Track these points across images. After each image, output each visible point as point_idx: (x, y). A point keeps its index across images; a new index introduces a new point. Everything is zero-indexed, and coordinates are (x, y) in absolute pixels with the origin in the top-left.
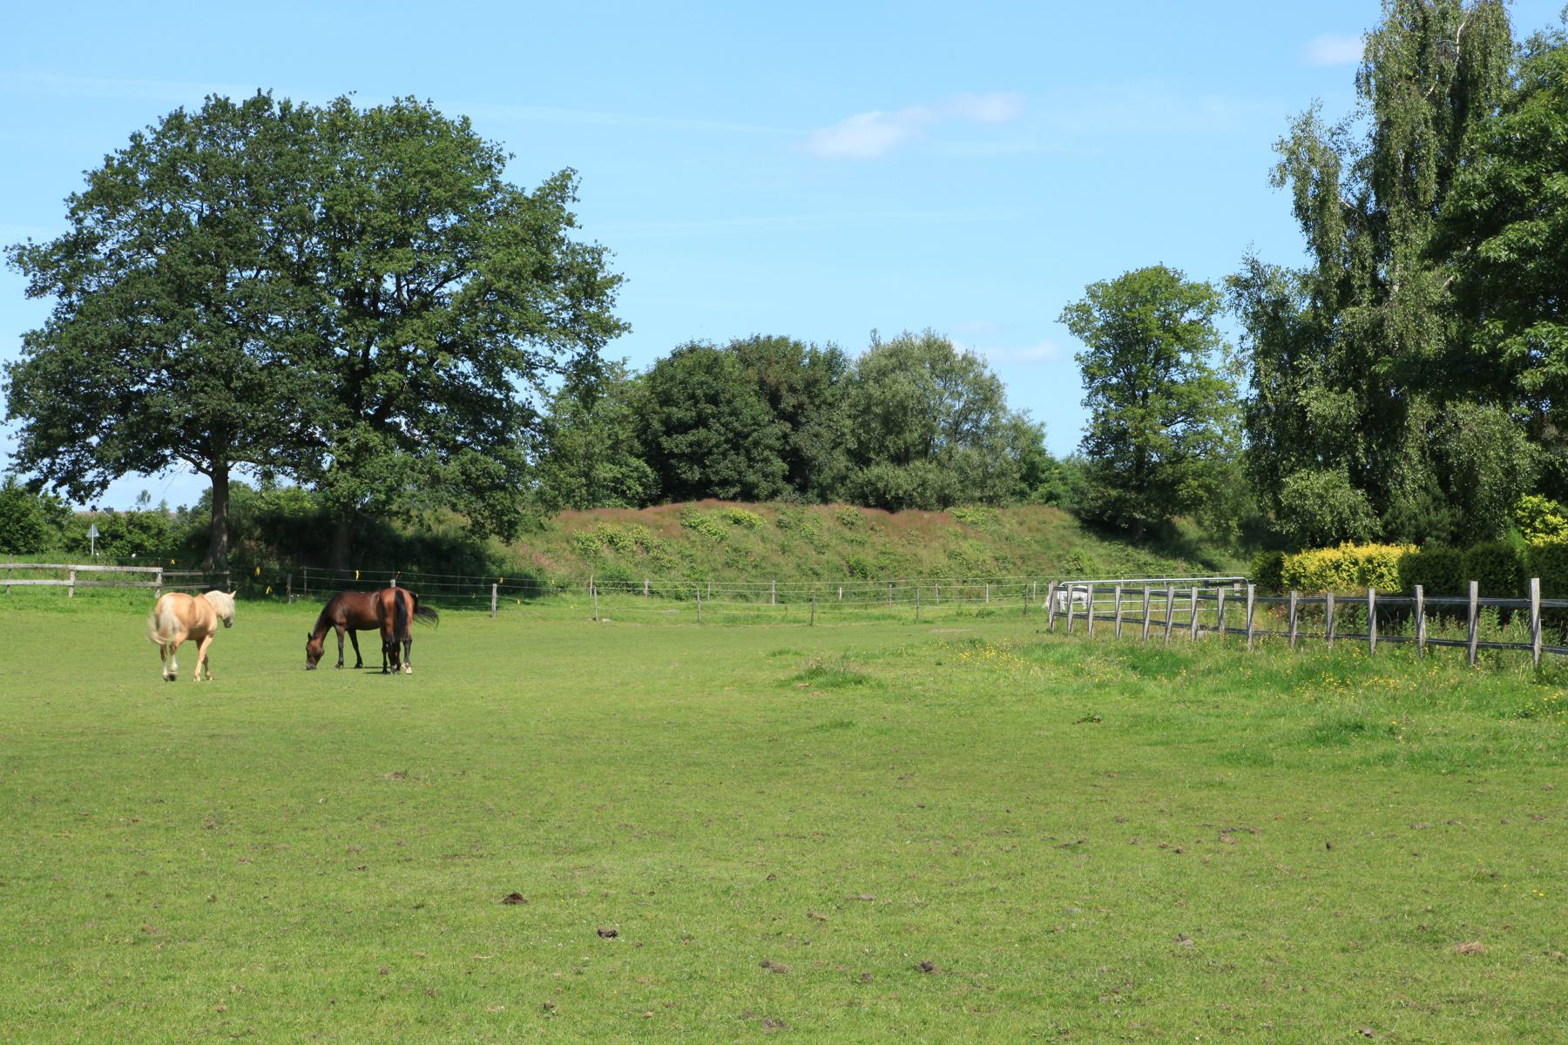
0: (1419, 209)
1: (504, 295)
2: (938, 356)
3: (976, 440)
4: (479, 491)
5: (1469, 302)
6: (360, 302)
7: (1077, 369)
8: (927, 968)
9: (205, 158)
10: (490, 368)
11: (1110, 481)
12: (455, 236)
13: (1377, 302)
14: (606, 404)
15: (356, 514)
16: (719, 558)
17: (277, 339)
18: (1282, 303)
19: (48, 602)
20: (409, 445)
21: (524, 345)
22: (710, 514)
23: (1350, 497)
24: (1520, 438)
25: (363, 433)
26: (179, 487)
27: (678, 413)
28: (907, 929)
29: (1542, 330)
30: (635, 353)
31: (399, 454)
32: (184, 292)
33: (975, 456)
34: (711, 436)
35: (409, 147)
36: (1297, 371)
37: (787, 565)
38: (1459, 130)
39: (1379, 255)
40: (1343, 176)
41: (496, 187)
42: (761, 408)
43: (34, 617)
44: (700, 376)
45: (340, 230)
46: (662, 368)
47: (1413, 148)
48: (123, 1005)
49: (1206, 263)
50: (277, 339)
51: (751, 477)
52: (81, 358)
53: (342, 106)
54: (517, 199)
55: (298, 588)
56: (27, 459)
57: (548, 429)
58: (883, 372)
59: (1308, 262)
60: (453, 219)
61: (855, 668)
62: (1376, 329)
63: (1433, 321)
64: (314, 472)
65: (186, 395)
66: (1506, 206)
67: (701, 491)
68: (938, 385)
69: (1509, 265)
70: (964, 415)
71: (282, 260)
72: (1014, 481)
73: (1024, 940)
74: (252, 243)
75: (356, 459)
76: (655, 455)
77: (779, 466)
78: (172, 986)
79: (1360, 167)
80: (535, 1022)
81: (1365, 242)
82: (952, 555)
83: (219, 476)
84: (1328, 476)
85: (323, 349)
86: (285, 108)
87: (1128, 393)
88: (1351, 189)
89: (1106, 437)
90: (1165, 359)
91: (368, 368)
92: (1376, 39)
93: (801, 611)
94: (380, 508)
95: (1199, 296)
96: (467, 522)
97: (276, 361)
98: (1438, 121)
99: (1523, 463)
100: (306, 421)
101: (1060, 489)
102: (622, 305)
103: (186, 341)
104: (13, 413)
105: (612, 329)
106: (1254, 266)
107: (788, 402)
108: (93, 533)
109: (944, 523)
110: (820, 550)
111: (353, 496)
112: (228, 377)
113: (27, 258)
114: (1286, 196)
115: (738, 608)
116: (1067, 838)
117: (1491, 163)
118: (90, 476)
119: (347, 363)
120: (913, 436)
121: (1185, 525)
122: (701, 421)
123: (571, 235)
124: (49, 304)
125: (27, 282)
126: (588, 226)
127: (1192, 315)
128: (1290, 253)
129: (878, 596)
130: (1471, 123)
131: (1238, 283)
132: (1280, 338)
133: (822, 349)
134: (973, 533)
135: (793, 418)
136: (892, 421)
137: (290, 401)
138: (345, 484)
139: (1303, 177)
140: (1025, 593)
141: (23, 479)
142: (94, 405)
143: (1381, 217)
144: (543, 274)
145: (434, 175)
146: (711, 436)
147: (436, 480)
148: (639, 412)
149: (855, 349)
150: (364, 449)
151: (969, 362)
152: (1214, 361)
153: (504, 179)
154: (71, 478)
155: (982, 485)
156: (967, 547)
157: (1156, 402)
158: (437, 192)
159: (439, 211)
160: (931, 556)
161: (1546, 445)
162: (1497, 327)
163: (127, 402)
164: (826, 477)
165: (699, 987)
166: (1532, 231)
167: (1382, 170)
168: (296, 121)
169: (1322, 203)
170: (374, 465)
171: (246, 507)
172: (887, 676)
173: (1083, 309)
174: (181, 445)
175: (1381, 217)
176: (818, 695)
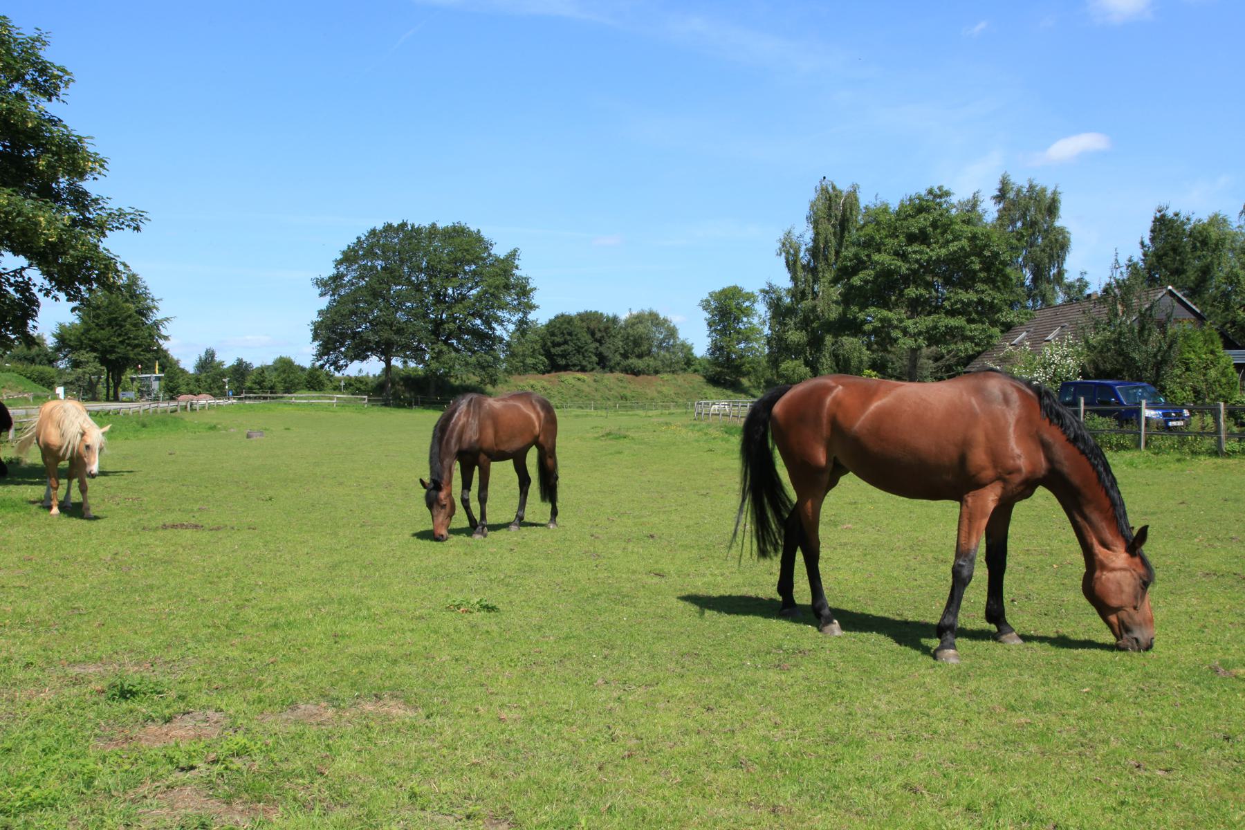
0: (829, 265)
1: (492, 295)
2: (654, 318)
3: (668, 350)
4: (483, 368)
5: (847, 299)
6: (439, 298)
7: (705, 323)
8: (652, 536)
9: (383, 245)
10: (487, 322)
11: (719, 365)
12: (474, 273)
13: (814, 299)
14: (530, 336)
15: (438, 377)
16: (572, 393)
17: (409, 312)
18: (779, 299)
19: (326, 408)
20: (457, 351)
21: (500, 313)
22: (569, 377)
23: (804, 370)
24: (864, 349)
25: (440, 346)
26: (373, 367)
27: (557, 339)
28: (643, 524)
29: (871, 310)
30: (541, 317)
31: (453, 354)
32: (375, 294)
33: (668, 356)
34: (570, 348)
35: (458, 241)
36: (785, 325)
37: (598, 395)
38: (842, 237)
39: (815, 282)
40: (802, 254)
41: (490, 255)
42: (588, 338)
43: (322, 414)
44: (565, 326)
45: (432, 271)
46: (551, 322)
47: (826, 242)
48: (358, 547)
49: (752, 285)
50: (409, 312)
51: (584, 363)
52: (339, 319)
53: (434, 226)
54: (497, 259)
55: (416, 404)
56: (319, 356)
57: (508, 345)
58: (633, 324)
59: (790, 285)
60: (474, 267)
61: (623, 432)
62: (814, 308)
63: (833, 306)
64: (422, 361)
65: (376, 333)
66: (860, 265)
67: (566, 368)
68: (654, 329)
69: (861, 287)
70: (663, 340)
71: (410, 282)
72: (682, 364)
73: (688, 527)
74: (400, 276)
75: (438, 356)
76: (548, 355)
77: (595, 359)
78: (376, 541)
79: (807, 250)
80: (507, 555)
81: (810, 277)
82: (659, 392)
83: (388, 362)
84: (797, 362)
85: (426, 315)
86: (413, 226)
87: (724, 332)
88: (804, 257)
89: (716, 348)
90: (737, 320)
91: (442, 322)
92: (813, 205)
93: (603, 413)
94: (447, 374)
95: (750, 297)
96: (478, 379)
97: (409, 320)
98: (835, 234)
99: (865, 358)
100: (419, 342)
101: (699, 368)
102: (536, 299)
103: (376, 313)
104: (314, 339)
105: (533, 307)
106: (770, 286)
107: (598, 335)
108: (343, 384)
109: (656, 380)
110: (610, 390)
111: (438, 370)
112: (391, 325)
113: (321, 283)
114: (782, 260)
115: (579, 412)
116: (704, 492)
117: (853, 250)
118: (341, 362)
119: (434, 321)
120: (644, 348)
121: (745, 381)
122: (566, 342)
123: (517, 273)
124: (327, 299)
125: (319, 291)
126: (523, 269)
127: (747, 304)
128: (783, 281)
129: (631, 407)
130: (846, 234)
131: (763, 291)
132: (779, 312)
133: (611, 315)
134: (666, 384)
135: (600, 341)
136: (637, 342)
137: (414, 334)
138: (434, 365)
139: (788, 253)
140: (686, 406)
141: (318, 364)
142: (343, 336)
143: (815, 268)
144: (507, 287)
145: (467, 250)
146: (570, 348)
147: (467, 364)
148: (543, 339)
149: (623, 316)
150: (440, 352)
151: (665, 320)
152: (755, 321)
153: (492, 252)
154: (335, 363)
155: (670, 366)
156: (665, 389)
157: (735, 336)
158: (468, 257)
159: (469, 263)
160: (651, 392)
161: (873, 351)
162: (856, 309)
163: (355, 335)
164: (612, 363)
165: (567, 543)
166: (868, 274)
167: (814, 252)
168: (417, 231)
169: (795, 262)
170: (445, 358)
171: (397, 374)
172: (636, 435)
173: (707, 301)
174: (374, 351)
175: (815, 268)
176: (609, 442)
